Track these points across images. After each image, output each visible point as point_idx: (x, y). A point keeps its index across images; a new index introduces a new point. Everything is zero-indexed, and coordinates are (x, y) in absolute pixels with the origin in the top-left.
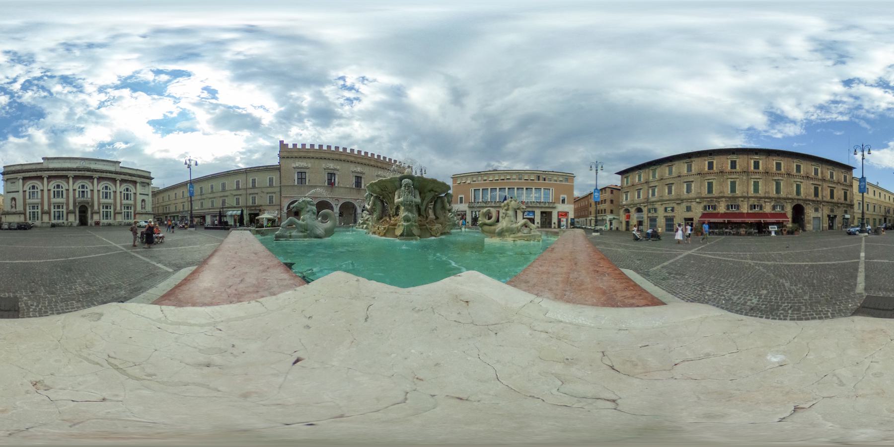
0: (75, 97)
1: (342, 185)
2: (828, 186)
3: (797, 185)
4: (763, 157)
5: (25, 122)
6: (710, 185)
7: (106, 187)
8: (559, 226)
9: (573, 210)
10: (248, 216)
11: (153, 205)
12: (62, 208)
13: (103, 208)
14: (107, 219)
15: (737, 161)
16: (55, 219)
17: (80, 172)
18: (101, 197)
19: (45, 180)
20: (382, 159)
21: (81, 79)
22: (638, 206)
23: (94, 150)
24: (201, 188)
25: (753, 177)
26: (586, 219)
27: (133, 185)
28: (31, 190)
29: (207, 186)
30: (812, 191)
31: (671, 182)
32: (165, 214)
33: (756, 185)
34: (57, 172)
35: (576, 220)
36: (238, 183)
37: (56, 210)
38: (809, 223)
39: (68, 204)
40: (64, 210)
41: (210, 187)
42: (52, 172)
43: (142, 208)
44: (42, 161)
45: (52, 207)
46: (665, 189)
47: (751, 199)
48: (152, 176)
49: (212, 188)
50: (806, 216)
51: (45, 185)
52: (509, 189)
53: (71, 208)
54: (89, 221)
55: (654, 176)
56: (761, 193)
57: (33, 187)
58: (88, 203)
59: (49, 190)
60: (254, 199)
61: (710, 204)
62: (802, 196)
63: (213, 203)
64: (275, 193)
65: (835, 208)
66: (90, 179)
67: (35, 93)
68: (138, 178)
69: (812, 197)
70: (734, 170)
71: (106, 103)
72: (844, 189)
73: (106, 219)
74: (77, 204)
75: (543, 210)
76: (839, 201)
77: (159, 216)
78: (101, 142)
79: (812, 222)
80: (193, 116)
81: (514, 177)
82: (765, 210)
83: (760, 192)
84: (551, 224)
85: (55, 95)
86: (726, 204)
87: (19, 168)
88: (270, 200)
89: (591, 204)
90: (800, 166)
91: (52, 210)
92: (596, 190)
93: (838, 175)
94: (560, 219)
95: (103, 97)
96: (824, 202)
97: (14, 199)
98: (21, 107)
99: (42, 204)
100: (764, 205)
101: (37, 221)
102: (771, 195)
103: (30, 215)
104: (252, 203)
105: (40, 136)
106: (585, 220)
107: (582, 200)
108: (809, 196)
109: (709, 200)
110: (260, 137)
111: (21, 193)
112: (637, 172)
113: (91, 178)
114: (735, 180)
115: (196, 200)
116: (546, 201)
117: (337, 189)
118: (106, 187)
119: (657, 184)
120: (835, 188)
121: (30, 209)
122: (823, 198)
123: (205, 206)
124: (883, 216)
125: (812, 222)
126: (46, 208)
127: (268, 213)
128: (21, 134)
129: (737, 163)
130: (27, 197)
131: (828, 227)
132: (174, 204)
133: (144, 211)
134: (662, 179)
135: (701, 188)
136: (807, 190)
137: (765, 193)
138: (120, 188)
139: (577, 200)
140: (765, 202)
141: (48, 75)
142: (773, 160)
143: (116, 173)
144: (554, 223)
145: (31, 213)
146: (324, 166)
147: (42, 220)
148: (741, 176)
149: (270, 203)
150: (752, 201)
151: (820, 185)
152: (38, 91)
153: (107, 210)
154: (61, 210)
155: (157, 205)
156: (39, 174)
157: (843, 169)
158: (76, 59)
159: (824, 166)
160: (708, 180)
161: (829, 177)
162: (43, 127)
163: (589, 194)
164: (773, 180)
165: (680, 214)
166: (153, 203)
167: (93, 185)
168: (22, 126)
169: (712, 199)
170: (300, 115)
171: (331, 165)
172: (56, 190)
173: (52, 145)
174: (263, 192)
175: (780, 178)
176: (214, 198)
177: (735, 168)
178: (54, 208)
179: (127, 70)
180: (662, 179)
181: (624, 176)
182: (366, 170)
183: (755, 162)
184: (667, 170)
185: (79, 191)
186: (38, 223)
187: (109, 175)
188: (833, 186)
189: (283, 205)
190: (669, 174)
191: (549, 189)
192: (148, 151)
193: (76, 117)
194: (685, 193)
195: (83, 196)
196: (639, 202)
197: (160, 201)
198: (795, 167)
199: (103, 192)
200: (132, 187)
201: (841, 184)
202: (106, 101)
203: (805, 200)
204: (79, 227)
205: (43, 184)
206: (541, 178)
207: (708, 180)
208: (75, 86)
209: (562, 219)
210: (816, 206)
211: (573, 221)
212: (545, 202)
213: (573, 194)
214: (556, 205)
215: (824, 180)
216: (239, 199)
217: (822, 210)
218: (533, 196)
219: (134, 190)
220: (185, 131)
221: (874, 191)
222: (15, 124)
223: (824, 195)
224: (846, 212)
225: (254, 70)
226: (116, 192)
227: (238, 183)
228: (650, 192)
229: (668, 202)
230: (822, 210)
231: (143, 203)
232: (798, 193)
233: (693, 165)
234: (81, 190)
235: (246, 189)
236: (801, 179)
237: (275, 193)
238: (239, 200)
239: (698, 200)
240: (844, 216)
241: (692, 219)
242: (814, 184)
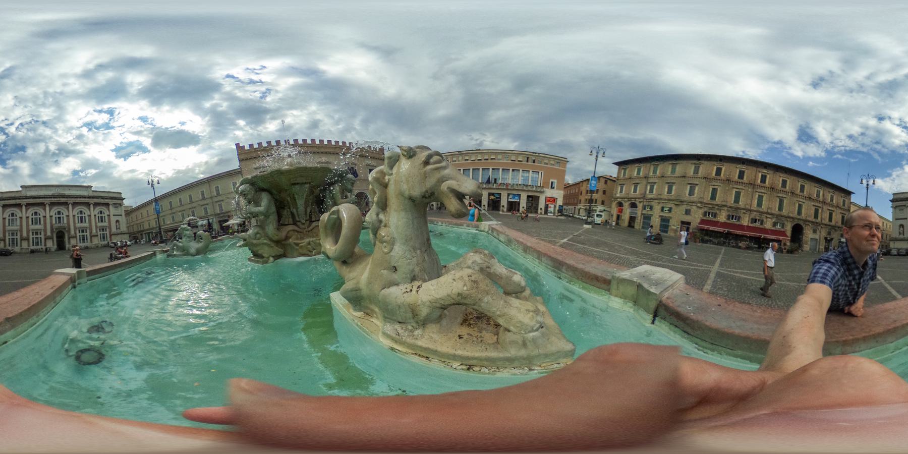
2: (828, 209)
3: (799, 205)
4: (771, 172)
6: (714, 191)
7: (81, 212)
8: (546, 212)
9: (562, 196)
11: (127, 224)
12: (41, 234)
14: (84, 242)
15: (746, 172)
16: (33, 245)
17: (56, 199)
18: (77, 221)
19: (24, 207)
22: (633, 201)
24: (170, 203)
25: (759, 190)
26: (575, 208)
27: (106, 208)
28: (11, 218)
29: (175, 200)
30: (813, 212)
31: (672, 181)
33: (760, 198)
35: (564, 207)
37: (35, 236)
38: (806, 243)
39: (45, 231)
40: (43, 236)
41: (178, 200)
43: (117, 229)
44: (21, 189)
45: (31, 234)
46: (665, 188)
47: (753, 213)
48: (123, 196)
50: (804, 237)
51: (23, 213)
52: (493, 169)
53: (49, 234)
54: (67, 246)
55: (655, 172)
56: (764, 208)
57: (13, 215)
58: (65, 228)
59: (27, 217)
61: (711, 211)
62: (803, 216)
63: (184, 215)
66: (65, 205)
68: (110, 201)
70: (740, 181)
72: (842, 213)
74: (54, 230)
75: (530, 194)
76: (837, 224)
77: (135, 234)
79: (809, 243)
81: (500, 157)
82: (765, 226)
83: (763, 206)
84: (537, 210)
86: (728, 214)
89: (581, 192)
90: (804, 186)
91: (31, 237)
92: (593, 178)
93: (838, 199)
94: (548, 205)
96: (822, 224)
99: (21, 231)
100: (765, 220)
102: (773, 212)
103: (9, 241)
104: (220, 210)
105: (25, 168)
106: (573, 209)
107: (572, 187)
109: (710, 206)
112: (637, 165)
113: (66, 204)
114: (740, 190)
115: (168, 214)
116: (534, 185)
118: (81, 212)
119: (657, 181)
120: (833, 211)
121: (9, 236)
122: (821, 221)
126: (25, 234)
129: (745, 174)
130: (7, 224)
131: (824, 250)
132: (148, 221)
133: (119, 231)
134: (663, 176)
135: (704, 193)
136: (808, 211)
137: (768, 209)
138: (94, 212)
139: (567, 187)
140: (767, 217)
142: (780, 176)
143: (89, 197)
144: (541, 209)
145: (11, 240)
147: (21, 246)
148: (747, 188)
150: (753, 215)
151: (820, 207)
153: (83, 234)
154: (39, 236)
155: (132, 224)
156: (18, 201)
160: (713, 185)
161: (829, 200)
163: (581, 182)
164: (777, 196)
165: (677, 216)
166: (127, 222)
169: (714, 206)
172: (34, 217)
175: (784, 196)
176: (184, 210)
177: (742, 179)
178: (33, 235)
180: (663, 176)
181: (622, 167)
183: (762, 175)
184: (670, 168)
185: (56, 217)
186: (17, 249)
187: (83, 200)
188: (833, 209)
190: (671, 173)
191: (539, 172)
192: (116, 174)
194: (687, 195)
195: (60, 222)
196: (635, 196)
198: (799, 186)
199: (78, 217)
201: (840, 208)
203: (806, 221)
204: (56, 252)
205: (22, 211)
206: (530, 160)
207: (713, 185)
209: (550, 205)
210: (815, 228)
211: (561, 207)
212: (533, 186)
213: (564, 178)
214: (544, 189)
215: (824, 202)
217: (820, 232)
218: (520, 178)
219: (89, 212)
223: (823, 217)
224: (842, 236)
226: (90, 216)
228: (649, 188)
229: (666, 202)
230: (820, 232)
231: (117, 224)
232: (799, 213)
233: (701, 167)
234: (57, 216)
235: (212, 198)
236: (803, 199)
238: (207, 209)
239: (699, 205)
240: (840, 239)
241: (689, 223)
242: (815, 206)
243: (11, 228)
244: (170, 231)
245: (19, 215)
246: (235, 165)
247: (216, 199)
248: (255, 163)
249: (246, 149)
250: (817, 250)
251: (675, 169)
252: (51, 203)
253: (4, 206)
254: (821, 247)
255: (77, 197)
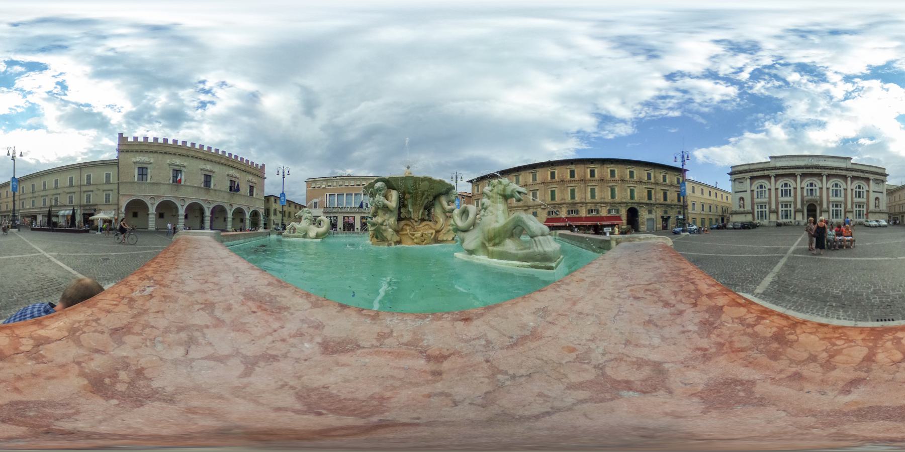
0: (816, 87)
1: (188, 184)
3: (631, 190)
5: (760, 115)
6: (553, 193)
7: (836, 185)
10: (82, 217)
12: (790, 207)
13: (833, 207)
14: (860, 218)
16: (782, 218)
17: (808, 170)
18: (831, 194)
19: (773, 179)
20: (233, 157)
21: (823, 67)
23: (837, 146)
24: (33, 186)
28: (759, 190)
29: (39, 183)
30: (646, 194)
32: (901, 213)
34: (784, 170)
36: (71, 179)
38: (643, 224)
39: (795, 203)
40: (792, 209)
42: (779, 171)
43: (875, 206)
48: (887, 172)
49: (45, 185)
53: (799, 206)
56: (597, 198)
57: (761, 186)
58: (817, 201)
60: (88, 198)
62: (636, 199)
64: (112, 190)
65: (669, 210)
66: (819, 177)
67: (768, 83)
68: (872, 175)
69: (646, 200)
71: (853, 94)
73: (836, 218)
78: (846, 138)
79: (646, 223)
80: (42, 112)
85: (792, 84)
87: (746, 168)
88: (106, 199)
90: (633, 172)
93: (671, 178)
95: (849, 87)
96: (658, 204)
97: (742, 199)
98: (755, 98)
99: (770, 203)
100: (600, 209)
101: (765, 221)
102: (606, 201)
103: (758, 214)
105: (778, 132)
108: (642, 198)
110: (106, 137)
111: (749, 191)
117: (183, 188)
118: (836, 185)
120: (668, 190)
122: (656, 201)
123: (36, 205)
124: (720, 215)
125: (646, 223)
126: (773, 207)
127: (105, 213)
128: (757, 129)
130: (755, 196)
131: (661, 228)
133: (877, 209)
136: (640, 194)
138: (852, 186)
140: (601, 207)
141: (781, 62)
143: (847, 169)
145: (759, 213)
146: (168, 161)
147: (769, 218)
149: (106, 202)
150: (589, 207)
152: (771, 80)
153: (837, 209)
155: (894, 204)
156: (766, 173)
157: (676, 172)
158: (813, 46)
159: (656, 170)
162: (781, 121)
167: (822, 183)
168: (757, 120)
170: (150, 116)
171: (178, 161)
172: (783, 188)
173: (792, 141)
174: (99, 190)
175: (614, 184)
179: (879, 60)
182: (217, 169)
185: (807, 189)
186: (765, 222)
187: (839, 172)
189: (120, 205)
193: (819, 109)
195: (812, 194)
197: (896, 200)
198: (628, 173)
199: (833, 190)
200: (865, 184)
201: (675, 186)
202: (853, 91)
203: (639, 204)
205: (770, 183)
208: (815, 76)
210: (650, 209)
215: (656, 184)
216: (72, 196)
217: (656, 212)
219: (867, 187)
220: (31, 127)
221: (716, 193)
222: (749, 118)
224: (679, 213)
225: (120, 67)
226: (846, 189)
227: (71, 179)
230: (656, 212)
231: (877, 202)
232: (632, 197)
235: (80, 186)
237: (112, 190)
239: (542, 207)
243: (759, 200)
244: (28, 217)
245: (768, 186)
246: (111, 155)
247: (84, 189)
248: (135, 157)
249: (159, 142)
250: (655, 229)
251: (519, 179)
252: (802, 174)
253: (752, 178)
254: (658, 226)
255: (832, 168)
